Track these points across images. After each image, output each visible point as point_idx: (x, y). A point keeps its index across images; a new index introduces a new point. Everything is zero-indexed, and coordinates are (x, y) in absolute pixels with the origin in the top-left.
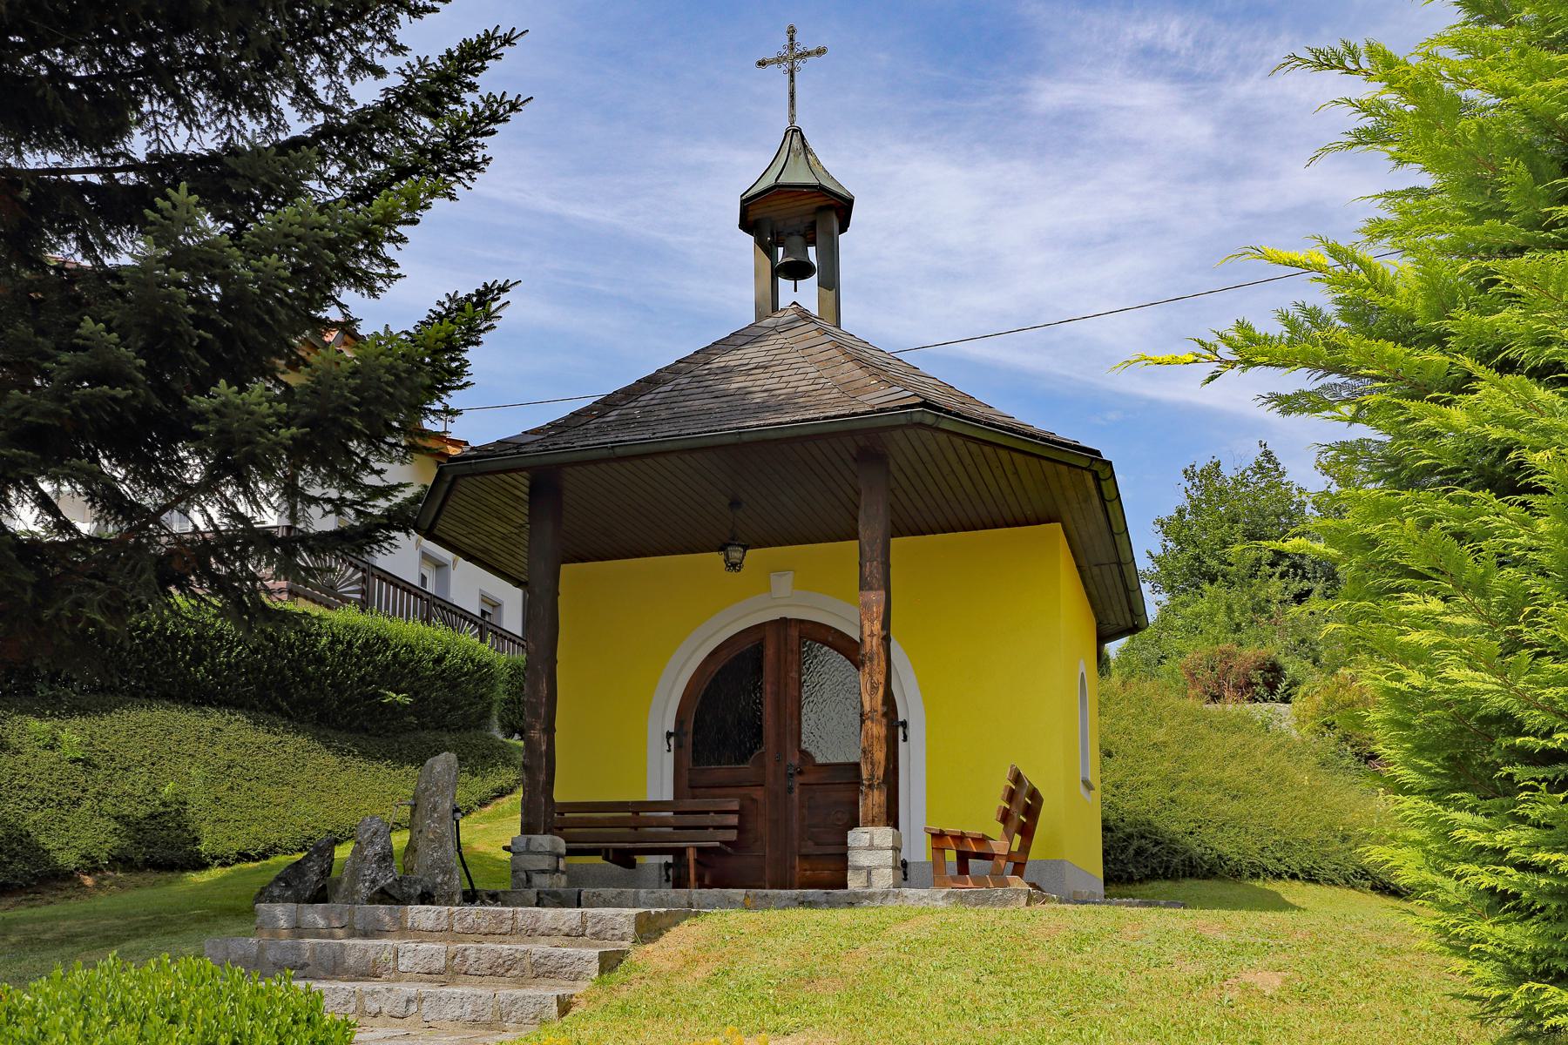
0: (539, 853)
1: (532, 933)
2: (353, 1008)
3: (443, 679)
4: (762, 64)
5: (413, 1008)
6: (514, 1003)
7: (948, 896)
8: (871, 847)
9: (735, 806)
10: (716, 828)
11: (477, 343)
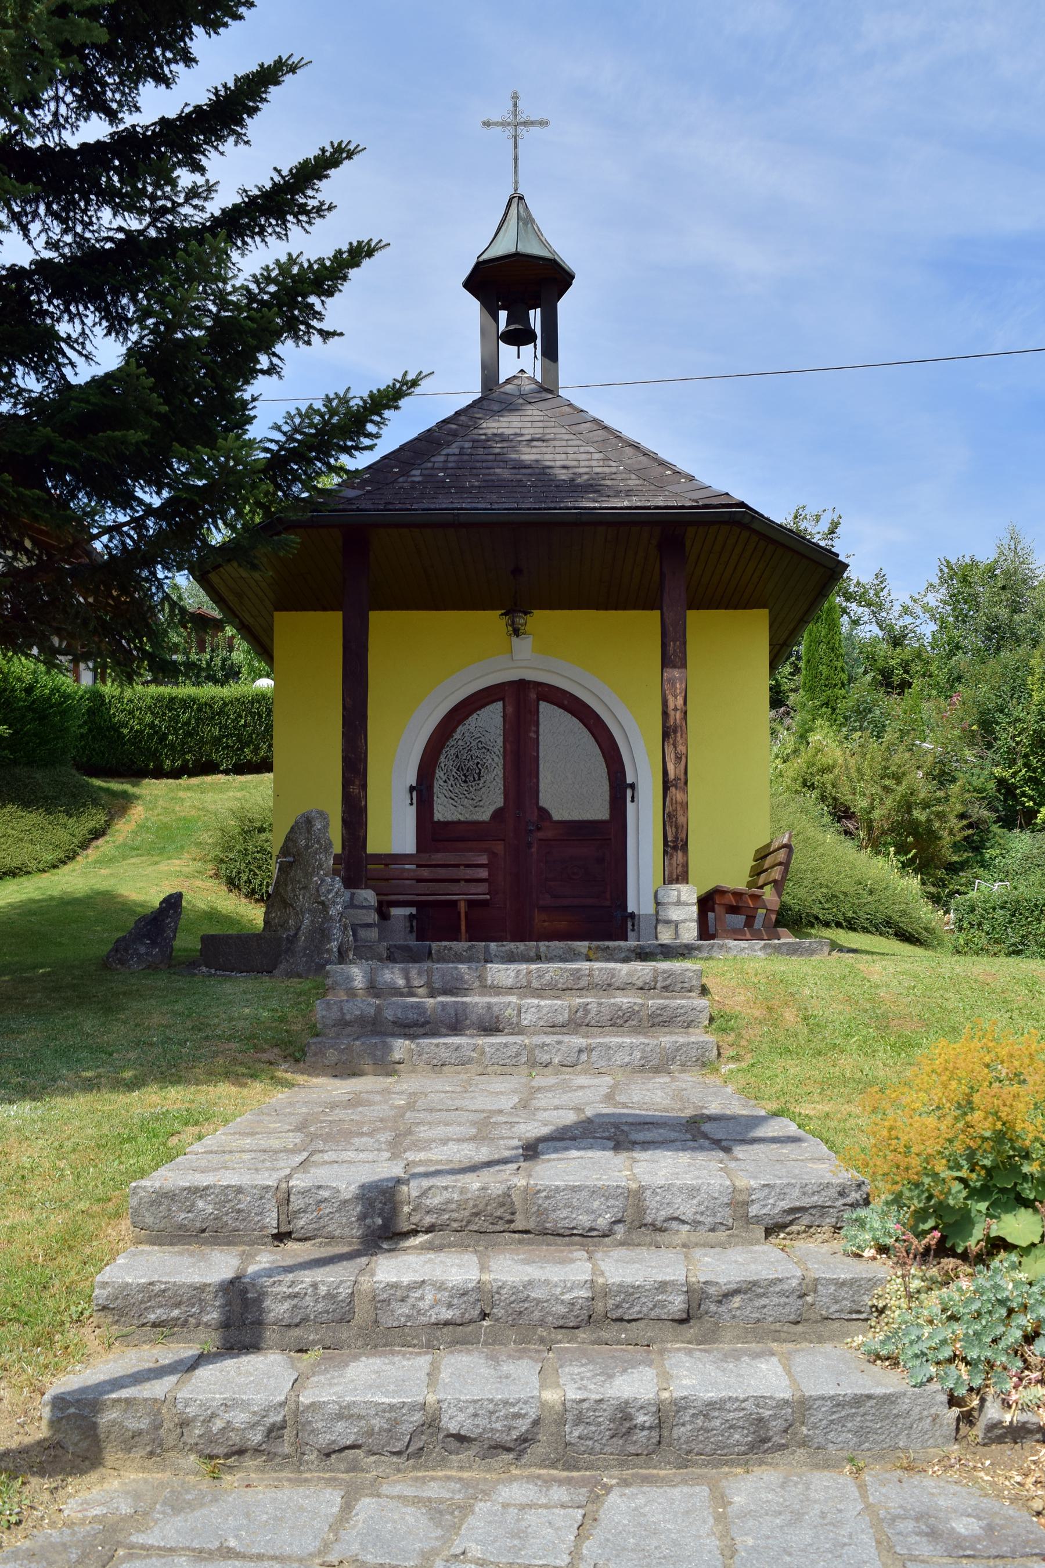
0: (364, 907)
1: (609, 987)
2: (524, 1059)
3: (34, 711)
4: (487, 124)
5: (584, 1057)
6: (678, 1049)
7: (764, 947)
8: (679, 903)
9: (483, 860)
10: (467, 881)
11: (397, 408)
